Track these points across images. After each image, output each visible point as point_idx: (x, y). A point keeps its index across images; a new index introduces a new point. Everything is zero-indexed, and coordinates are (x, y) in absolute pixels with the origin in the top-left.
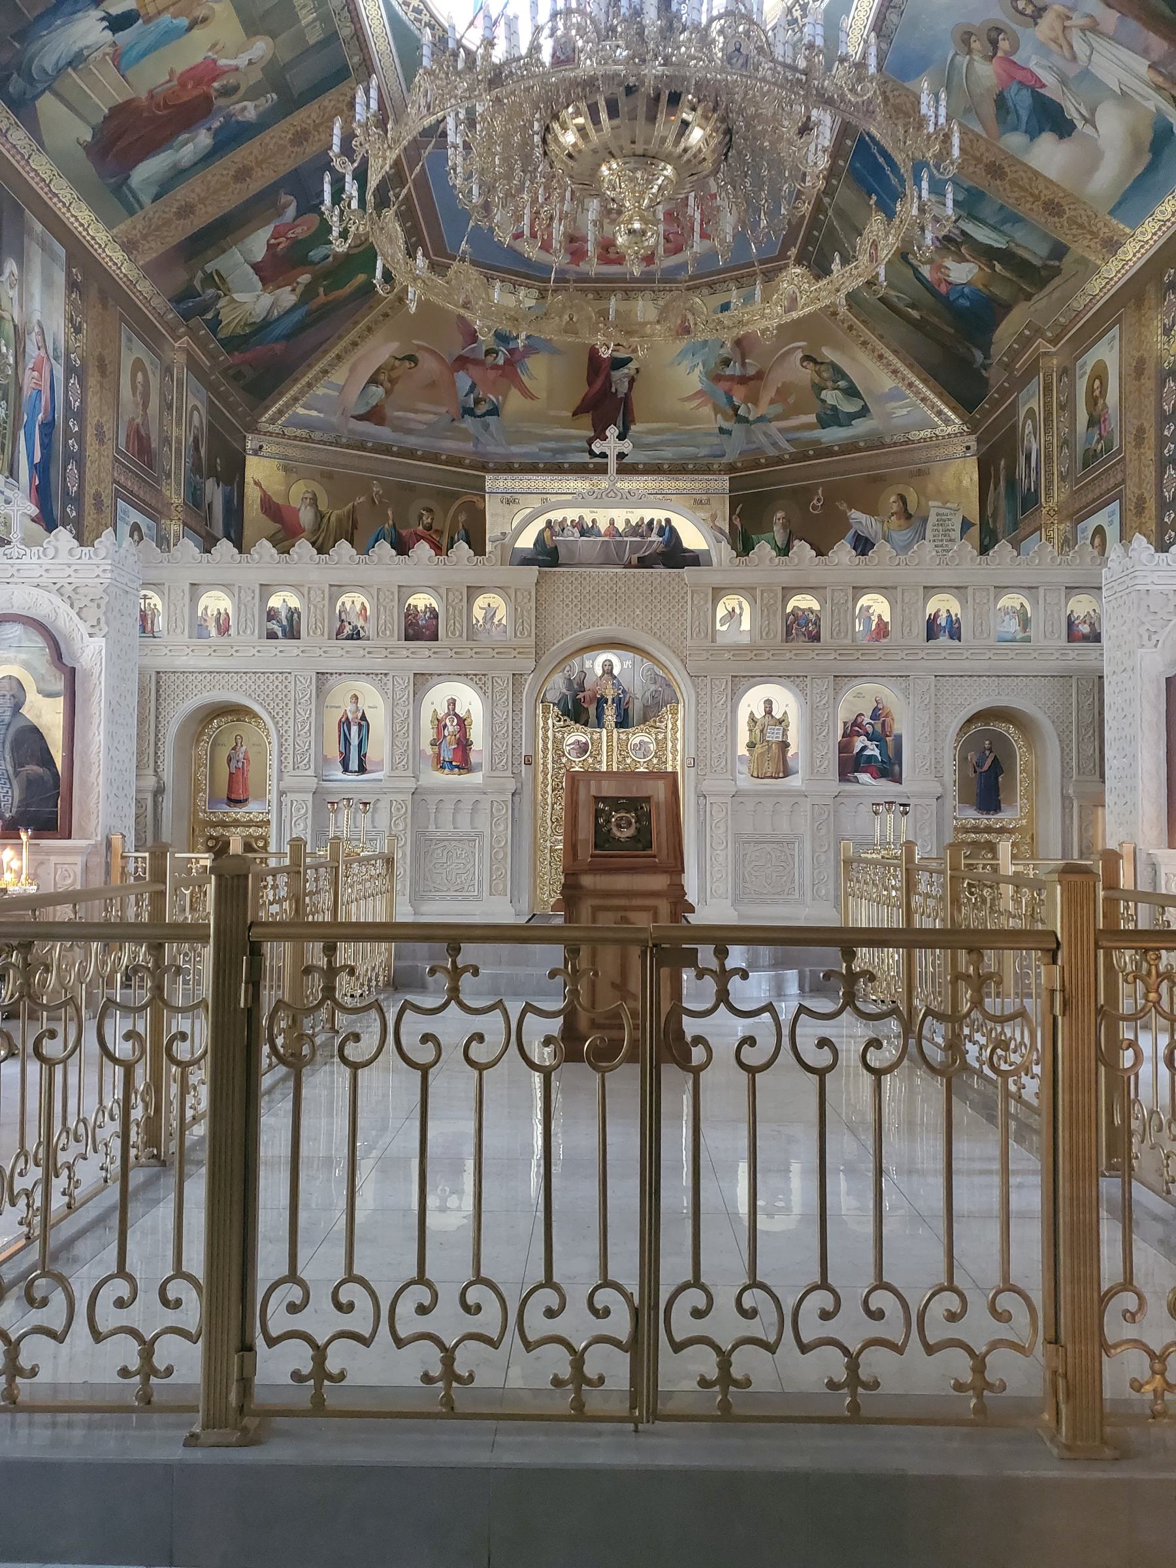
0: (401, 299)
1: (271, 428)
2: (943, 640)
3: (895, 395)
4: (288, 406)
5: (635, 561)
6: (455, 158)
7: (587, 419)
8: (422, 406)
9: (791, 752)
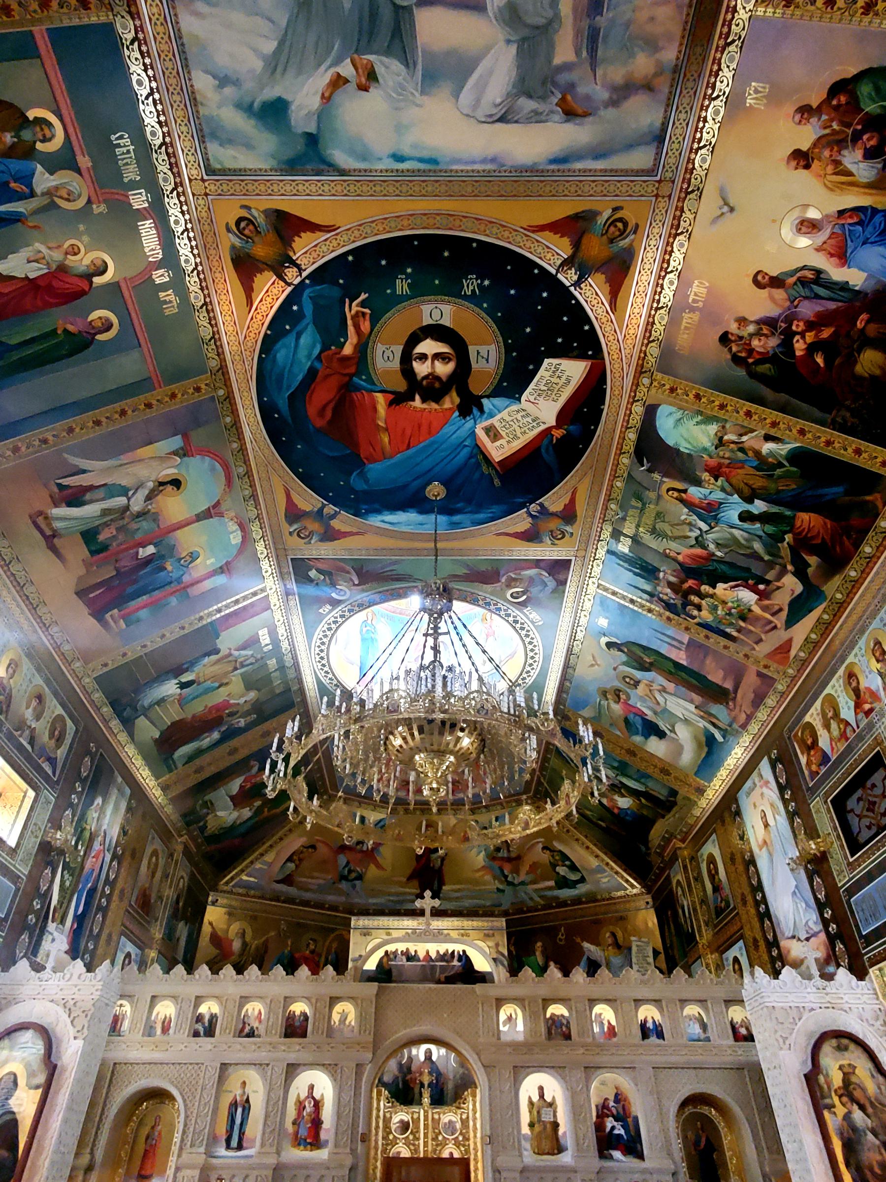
0: (303, 821)
1: (225, 888)
2: (653, 1039)
3: (599, 870)
4: (237, 874)
5: (443, 979)
6: (337, 752)
7: (416, 883)
8: (316, 874)
9: (560, 1132)
